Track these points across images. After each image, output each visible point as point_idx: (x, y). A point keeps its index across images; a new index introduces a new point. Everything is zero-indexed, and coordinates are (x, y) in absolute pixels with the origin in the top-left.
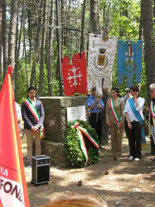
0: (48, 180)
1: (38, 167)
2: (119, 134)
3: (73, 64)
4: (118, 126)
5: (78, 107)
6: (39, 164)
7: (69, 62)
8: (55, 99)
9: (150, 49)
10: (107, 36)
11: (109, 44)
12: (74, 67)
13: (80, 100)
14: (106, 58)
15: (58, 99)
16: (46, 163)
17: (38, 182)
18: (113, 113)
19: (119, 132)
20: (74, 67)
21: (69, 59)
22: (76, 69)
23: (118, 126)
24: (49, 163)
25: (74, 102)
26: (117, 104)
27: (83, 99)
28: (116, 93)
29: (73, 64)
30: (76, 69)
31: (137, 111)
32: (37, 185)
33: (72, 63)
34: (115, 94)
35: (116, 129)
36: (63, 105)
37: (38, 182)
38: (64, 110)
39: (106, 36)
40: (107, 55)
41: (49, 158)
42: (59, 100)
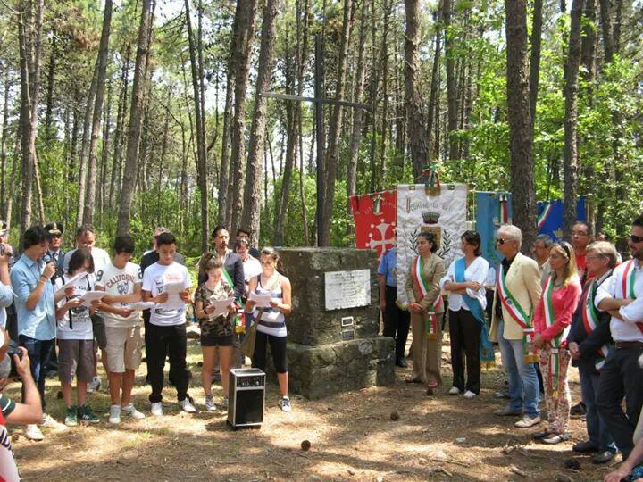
0: (261, 420)
1: (238, 392)
2: (432, 335)
3: (382, 213)
4: (431, 318)
5: (354, 271)
6: (240, 384)
7: (374, 210)
8: (301, 252)
9: (522, 148)
10: (439, 185)
11: (445, 201)
12: (383, 220)
13: (358, 257)
14: (443, 232)
15: (306, 252)
16: (256, 386)
17: (236, 423)
18: (420, 288)
19: (432, 332)
20: (383, 220)
21: (374, 203)
22: (388, 225)
23: (431, 318)
24: (263, 385)
25: (343, 260)
26: (428, 269)
27: (367, 255)
28: (427, 242)
29: (382, 213)
30: (388, 225)
31: (399, 310)
32: (236, 429)
33: (380, 211)
34: (425, 245)
35: (426, 324)
36: (316, 265)
37: (236, 423)
38: (317, 277)
39: (435, 186)
40: (443, 227)
41: (264, 374)
42: (307, 255)
